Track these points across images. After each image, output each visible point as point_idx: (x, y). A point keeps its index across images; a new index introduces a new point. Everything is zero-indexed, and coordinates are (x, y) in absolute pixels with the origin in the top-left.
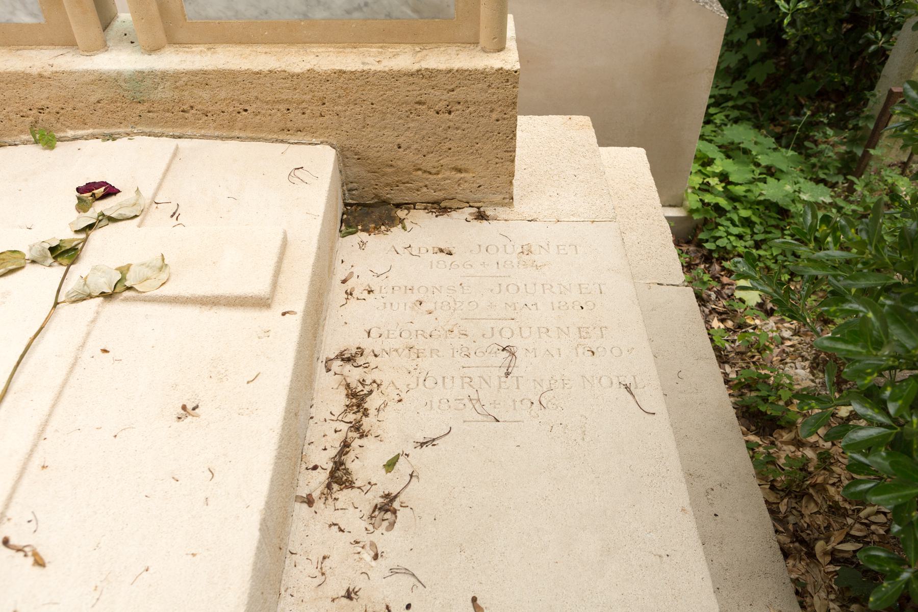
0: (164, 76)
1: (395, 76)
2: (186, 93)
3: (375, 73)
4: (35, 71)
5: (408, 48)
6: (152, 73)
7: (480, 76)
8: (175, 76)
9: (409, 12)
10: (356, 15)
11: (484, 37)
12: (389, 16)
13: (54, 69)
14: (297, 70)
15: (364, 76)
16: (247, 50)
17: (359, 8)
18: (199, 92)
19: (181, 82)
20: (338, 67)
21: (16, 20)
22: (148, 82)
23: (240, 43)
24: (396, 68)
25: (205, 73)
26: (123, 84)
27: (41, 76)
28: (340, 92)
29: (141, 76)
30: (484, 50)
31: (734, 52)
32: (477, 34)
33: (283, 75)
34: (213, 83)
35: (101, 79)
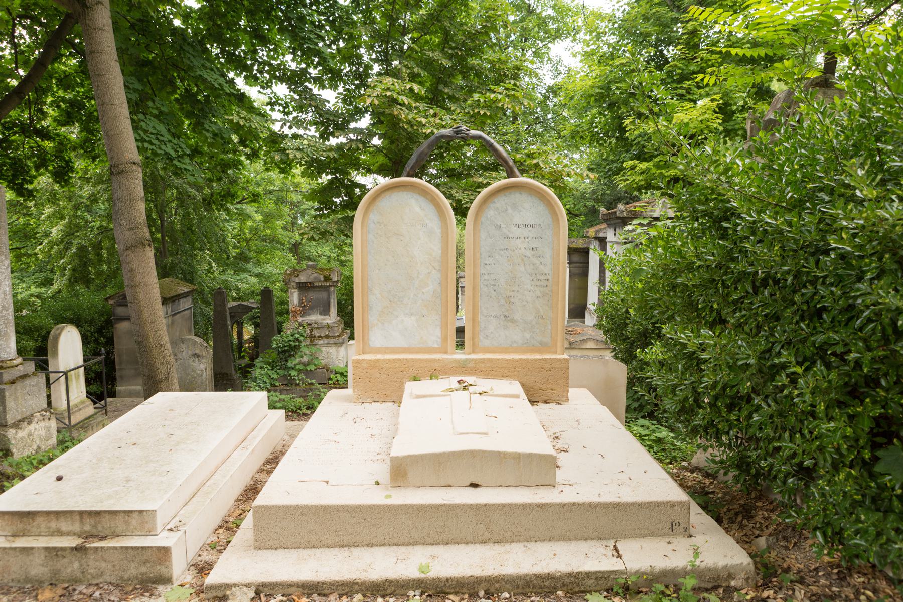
0: (473, 360)
1: (536, 360)
6: (470, 359)
7: (560, 360)
8: (476, 360)
11: (559, 350)
35: (455, 361)
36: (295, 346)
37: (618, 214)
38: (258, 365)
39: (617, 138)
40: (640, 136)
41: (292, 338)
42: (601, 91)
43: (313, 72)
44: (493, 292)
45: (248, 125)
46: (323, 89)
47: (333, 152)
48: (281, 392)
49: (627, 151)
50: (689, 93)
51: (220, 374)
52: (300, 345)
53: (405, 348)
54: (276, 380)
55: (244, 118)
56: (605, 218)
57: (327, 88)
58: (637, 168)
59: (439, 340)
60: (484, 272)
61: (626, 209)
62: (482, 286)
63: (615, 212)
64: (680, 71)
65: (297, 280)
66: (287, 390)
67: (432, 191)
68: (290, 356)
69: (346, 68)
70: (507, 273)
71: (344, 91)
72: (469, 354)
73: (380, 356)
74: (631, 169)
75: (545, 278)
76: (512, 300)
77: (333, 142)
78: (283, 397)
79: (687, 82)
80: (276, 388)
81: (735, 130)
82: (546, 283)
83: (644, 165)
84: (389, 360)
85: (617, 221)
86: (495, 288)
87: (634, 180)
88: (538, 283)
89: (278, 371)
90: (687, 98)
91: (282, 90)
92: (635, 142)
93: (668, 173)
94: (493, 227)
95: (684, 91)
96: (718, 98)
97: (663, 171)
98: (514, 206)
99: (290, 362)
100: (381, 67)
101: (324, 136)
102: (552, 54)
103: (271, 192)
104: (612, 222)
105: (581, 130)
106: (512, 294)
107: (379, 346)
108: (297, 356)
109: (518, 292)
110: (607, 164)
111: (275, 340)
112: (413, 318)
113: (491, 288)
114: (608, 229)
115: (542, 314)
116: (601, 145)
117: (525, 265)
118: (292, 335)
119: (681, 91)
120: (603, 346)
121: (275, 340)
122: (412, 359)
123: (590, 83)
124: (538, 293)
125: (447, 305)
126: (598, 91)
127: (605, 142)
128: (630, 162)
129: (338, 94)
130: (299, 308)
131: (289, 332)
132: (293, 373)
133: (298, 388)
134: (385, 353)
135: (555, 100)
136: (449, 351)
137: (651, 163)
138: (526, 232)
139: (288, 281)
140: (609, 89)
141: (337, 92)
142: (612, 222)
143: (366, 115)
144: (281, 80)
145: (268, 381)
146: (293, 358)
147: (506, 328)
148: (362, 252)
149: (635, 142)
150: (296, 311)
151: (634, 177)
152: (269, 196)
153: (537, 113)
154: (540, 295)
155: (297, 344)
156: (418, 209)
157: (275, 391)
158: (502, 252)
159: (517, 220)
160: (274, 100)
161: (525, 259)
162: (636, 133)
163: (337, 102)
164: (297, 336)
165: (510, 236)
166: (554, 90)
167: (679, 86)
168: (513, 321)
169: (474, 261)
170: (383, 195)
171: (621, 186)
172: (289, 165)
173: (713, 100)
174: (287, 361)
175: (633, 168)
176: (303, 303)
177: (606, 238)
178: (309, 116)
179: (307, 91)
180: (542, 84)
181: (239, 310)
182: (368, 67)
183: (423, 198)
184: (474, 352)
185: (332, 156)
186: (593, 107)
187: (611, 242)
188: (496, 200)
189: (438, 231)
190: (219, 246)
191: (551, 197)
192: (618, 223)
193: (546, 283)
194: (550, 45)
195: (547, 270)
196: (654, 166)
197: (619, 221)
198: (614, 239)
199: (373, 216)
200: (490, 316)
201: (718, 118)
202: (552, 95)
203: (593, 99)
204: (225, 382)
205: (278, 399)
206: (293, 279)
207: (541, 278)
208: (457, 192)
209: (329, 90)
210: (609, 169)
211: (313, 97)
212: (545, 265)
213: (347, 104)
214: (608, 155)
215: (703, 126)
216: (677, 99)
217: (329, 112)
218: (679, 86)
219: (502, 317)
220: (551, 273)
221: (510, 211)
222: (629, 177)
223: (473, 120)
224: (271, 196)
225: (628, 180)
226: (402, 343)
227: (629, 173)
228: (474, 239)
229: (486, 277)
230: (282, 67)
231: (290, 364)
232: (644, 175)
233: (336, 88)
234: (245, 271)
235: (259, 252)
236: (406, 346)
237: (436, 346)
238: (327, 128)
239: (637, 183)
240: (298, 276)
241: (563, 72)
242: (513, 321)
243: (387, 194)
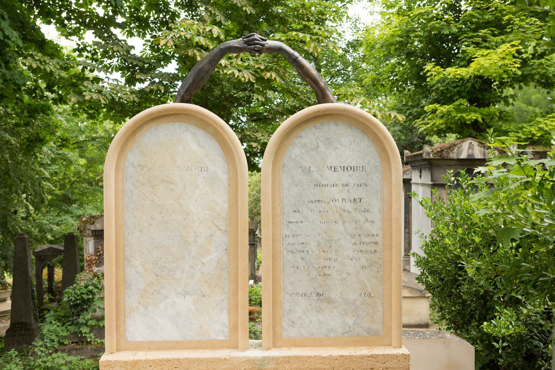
0: (273, 358)
1: (362, 357)
2: (280, 366)
3: (355, 356)
4: (223, 357)
5: (365, 347)
6: (269, 357)
7: (396, 357)
8: (277, 359)
9: (366, 334)
10: (346, 335)
11: (394, 342)
12: (358, 335)
13: (231, 356)
14: (325, 356)
15: (350, 358)
16: (303, 349)
17: (347, 332)
18: (285, 365)
19: (279, 361)
20: (341, 354)
21: (218, 338)
22: (267, 361)
23: (301, 346)
24: (363, 354)
25: (289, 357)
26: (256, 362)
27: (225, 359)
28: (341, 364)
29: (265, 359)
30: (394, 347)
31: (123, 123)
32: (391, 342)
33: (320, 357)
34: (292, 361)
35: (248, 360)
36: (88, 299)
37: (425, 156)
38: (48, 320)
39: (415, 85)
40: (438, 82)
41: (85, 291)
42: (401, 39)
43: (120, 19)
44: (300, 260)
45: (42, 67)
46: (131, 37)
47: (134, 96)
48: (69, 354)
49: (426, 97)
50: (485, 41)
51: (18, 324)
52: (93, 298)
53: (177, 342)
54: (66, 337)
55: (40, 60)
56: (410, 160)
57: (135, 36)
58: (439, 111)
59: (226, 330)
60: (288, 233)
61: (432, 151)
62: (285, 252)
63: (422, 154)
64: (477, 20)
65: (92, 228)
66: (76, 349)
67: (215, 122)
68: (83, 310)
69: (153, 16)
70: (319, 234)
71: (152, 37)
72: (269, 349)
73: (141, 356)
74: (432, 113)
75: (373, 240)
76: (327, 271)
77: (138, 86)
78: (71, 358)
79: (482, 31)
80: (63, 347)
81: (531, 74)
82: (373, 247)
83: (444, 109)
84: (153, 361)
85: (422, 163)
86: (304, 255)
87: (435, 124)
88: (363, 248)
89: (69, 327)
90: (483, 46)
91: (89, 37)
92: (434, 88)
93: (469, 117)
94: (300, 170)
95: (481, 39)
96: (516, 44)
97: (464, 115)
98: (328, 142)
99: (81, 317)
100: (186, 14)
101: (131, 81)
102: (350, 13)
103: (94, 139)
104: (417, 164)
105: (381, 78)
106: (327, 263)
107: (140, 339)
108: (90, 310)
109: (335, 260)
110: (408, 109)
111: (66, 293)
112: (189, 298)
113: (298, 256)
114: (413, 171)
115: (370, 291)
116: (400, 92)
117: (344, 222)
118: (86, 287)
119: (477, 39)
120: (418, 295)
121: (66, 293)
122: (187, 359)
123: (391, 32)
124: (364, 262)
125: (237, 280)
126: (398, 39)
127: (404, 89)
128: (431, 106)
129: (146, 41)
130: (94, 257)
131: (82, 284)
132: (84, 330)
133: (89, 347)
134: (149, 349)
135: (355, 54)
136: (240, 345)
137: (451, 106)
138: (344, 177)
139: (82, 228)
140: (408, 37)
141: (145, 39)
142: (417, 164)
143: (172, 61)
144: (88, 26)
145: (56, 339)
146: (85, 313)
147: (319, 311)
148: (116, 206)
149: (434, 88)
150: (91, 261)
151: (434, 121)
152: (91, 142)
153: (338, 66)
154: (365, 263)
155: (91, 296)
156: (194, 147)
157: (63, 351)
158: (312, 206)
159: (333, 161)
160: (82, 46)
161: (345, 214)
162: (437, 78)
163: (145, 49)
164: (91, 288)
165: (323, 182)
166: (354, 45)
167: (475, 34)
168: (330, 301)
169: (273, 218)
170: (146, 127)
171: (422, 129)
172: (97, 110)
173: (513, 46)
174: (79, 315)
175: (434, 111)
176: (98, 252)
177: (411, 180)
178: (115, 61)
179: (111, 35)
180: (343, 39)
181: (50, 254)
182: (174, 15)
183: (202, 131)
184: (275, 346)
185: (132, 100)
186: (393, 56)
187: (417, 184)
188: (303, 134)
189: (223, 177)
190: (34, 190)
191: (379, 129)
192: (424, 165)
193: (373, 247)
194: (348, 5)
195: (375, 229)
196: (454, 108)
197: (425, 163)
198: (420, 181)
199: (132, 157)
200: (297, 294)
201: (515, 62)
202: (351, 51)
203: (393, 48)
204: (23, 332)
205: (63, 362)
206: (88, 226)
207: (367, 240)
208: (262, 136)
209: (137, 38)
210: (410, 114)
211: (117, 41)
212: (373, 222)
213: (154, 51)
214: (407, 102)
215: (501, 71)
216: (474, 47)
217: (135, 57)
218: (475, 34)
219: (314, 295)
220: (380, 233)
221: (322, 148)
222: (429, 121)
223: (276, 60)
224: (93, 142)
225: (428, 124)
226: (173, 335)
227: (430, 117)
228: (273, 188)
229: (291, 240)
230: (93, 15)
231: (81, 320)
232: (445, 119)
233: (144, 35)
234: (67, 212)
235: (83, 194)
236: (179, 339)
237: (221, 338)
238: (133, 73)
239: (437, 127)
240: (94, 223)
241: (362, 29)
242: (330, 301)
243: (153, 125)
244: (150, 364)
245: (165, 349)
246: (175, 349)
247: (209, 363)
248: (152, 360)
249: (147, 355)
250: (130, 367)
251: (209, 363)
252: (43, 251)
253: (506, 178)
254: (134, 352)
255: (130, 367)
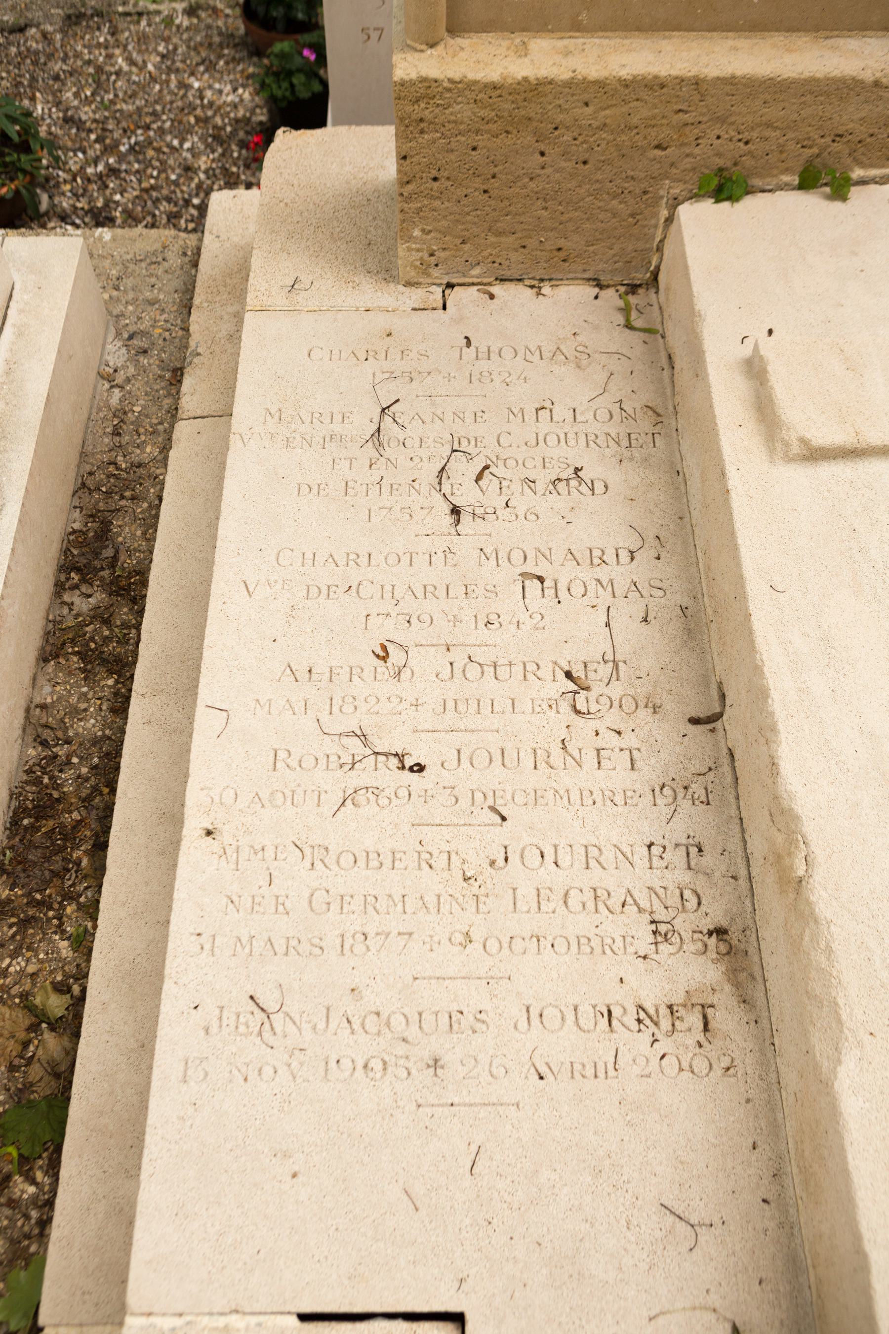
4: (868, 76)
84: (600, 84)
122: (731, 81)
244: (586, 97)
245: (639, 29)
246: (677, 28)
247: (808, 98)
248: (596, 82)
249: (567, 53)
250: (508, 106)
251: (808, 98)
252: (282, 40)
253: (70, 217)
254: (518, 38)
255: (508, 106)
